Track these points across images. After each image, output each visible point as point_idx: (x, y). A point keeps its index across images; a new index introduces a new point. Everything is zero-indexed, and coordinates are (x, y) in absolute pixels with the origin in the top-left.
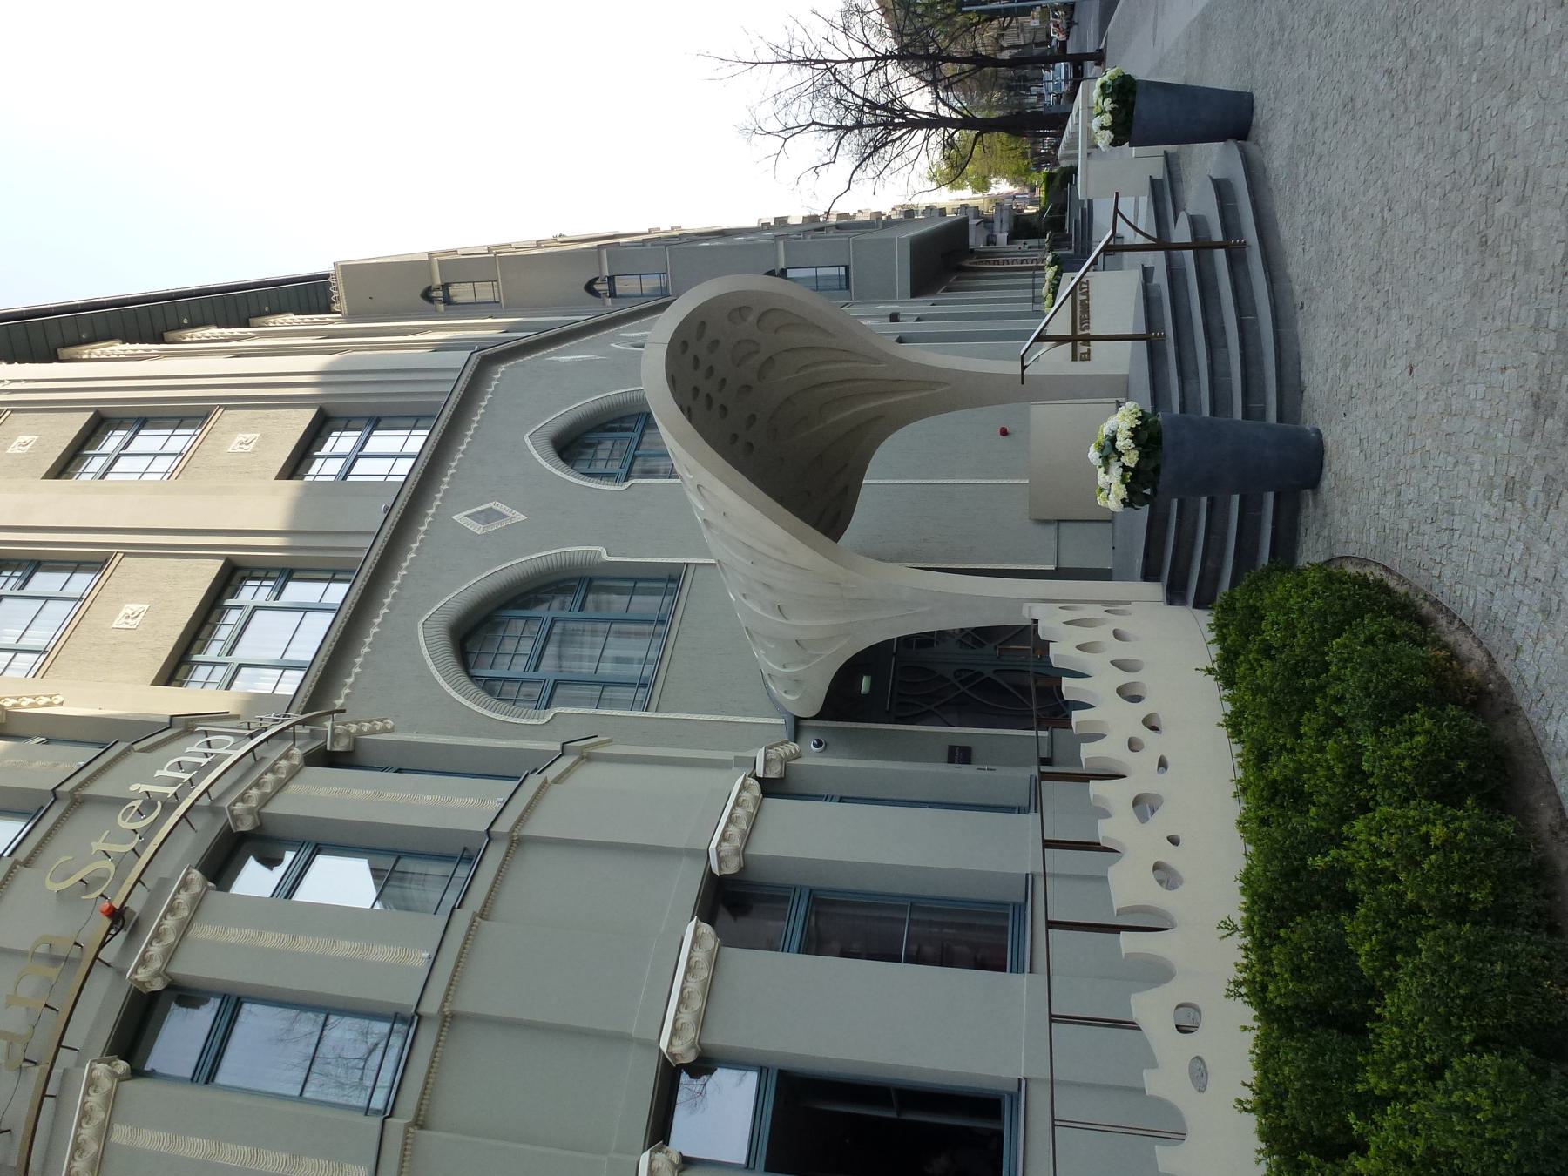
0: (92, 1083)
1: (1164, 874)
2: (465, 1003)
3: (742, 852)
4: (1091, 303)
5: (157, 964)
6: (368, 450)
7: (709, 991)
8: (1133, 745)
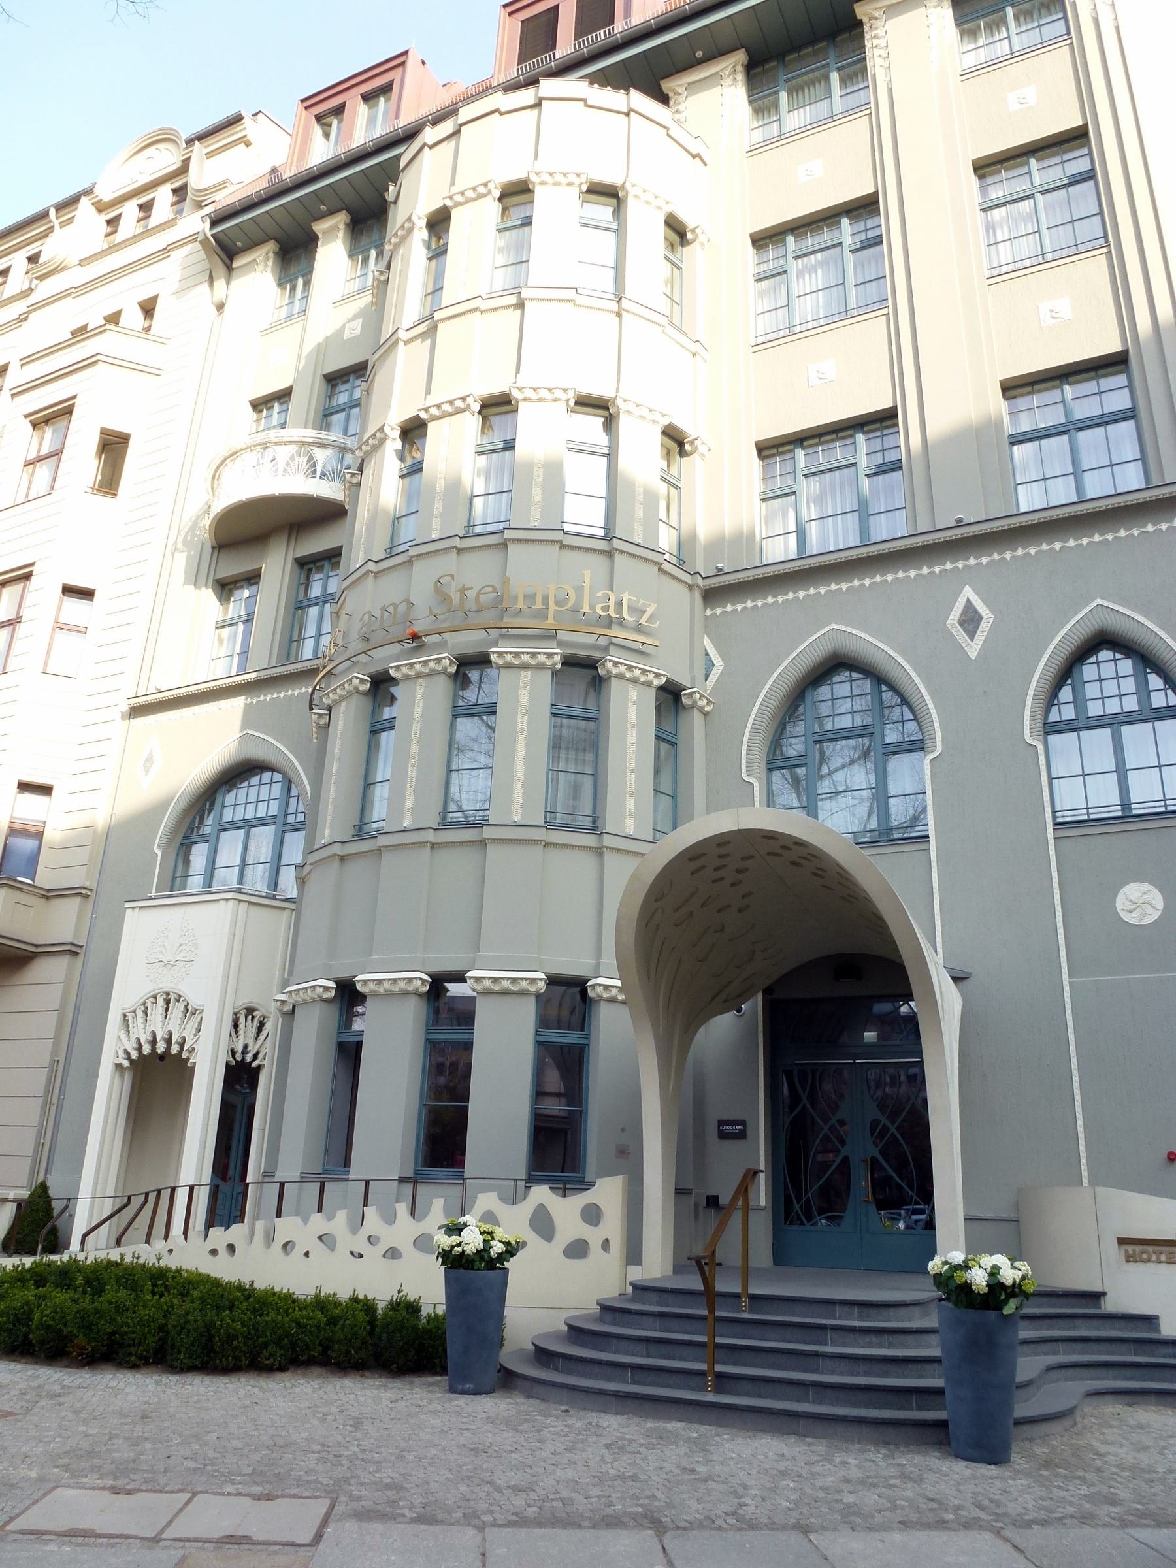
0: (439, 660)
2: (608, 856)
3: (600, 999)
5: (614, 671)
7: (506, 993)
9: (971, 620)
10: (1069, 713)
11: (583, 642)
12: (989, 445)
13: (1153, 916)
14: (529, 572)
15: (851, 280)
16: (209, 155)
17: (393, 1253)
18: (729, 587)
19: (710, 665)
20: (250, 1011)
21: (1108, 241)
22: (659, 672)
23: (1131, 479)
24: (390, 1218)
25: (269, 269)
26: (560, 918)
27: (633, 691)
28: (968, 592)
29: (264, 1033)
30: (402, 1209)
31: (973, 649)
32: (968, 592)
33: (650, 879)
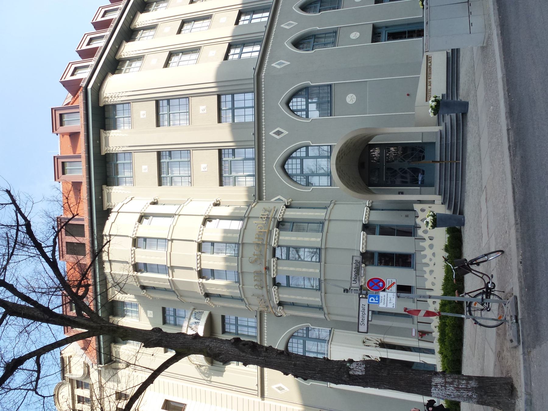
1: (433, 284)
3: (368, 220)
4: (432, 67)
6: (244, 51)
7: (366, 242)
8: (431, 260)
9: (278, 133)
10: (304, 113)
11: (272, 224)
12: (235, 127)
13: (354, 96)
14: (251, 238)
15: (180, 160)
16: (70, 372)
17: (434, 254)
18: (258, 194)
19: (279, 199)
20: (364, 342)
21: (187, 97)
22: (282, 207)
23: (250, 96)
24: (425, 256)
25: (120, 346)
26: (351, 213)
27: (286, 213)
28: (271, 133)
29: (370, 339)
30: (422, 253)
31: (286, 132)
32: (271, 133)
33: (344, 187)
